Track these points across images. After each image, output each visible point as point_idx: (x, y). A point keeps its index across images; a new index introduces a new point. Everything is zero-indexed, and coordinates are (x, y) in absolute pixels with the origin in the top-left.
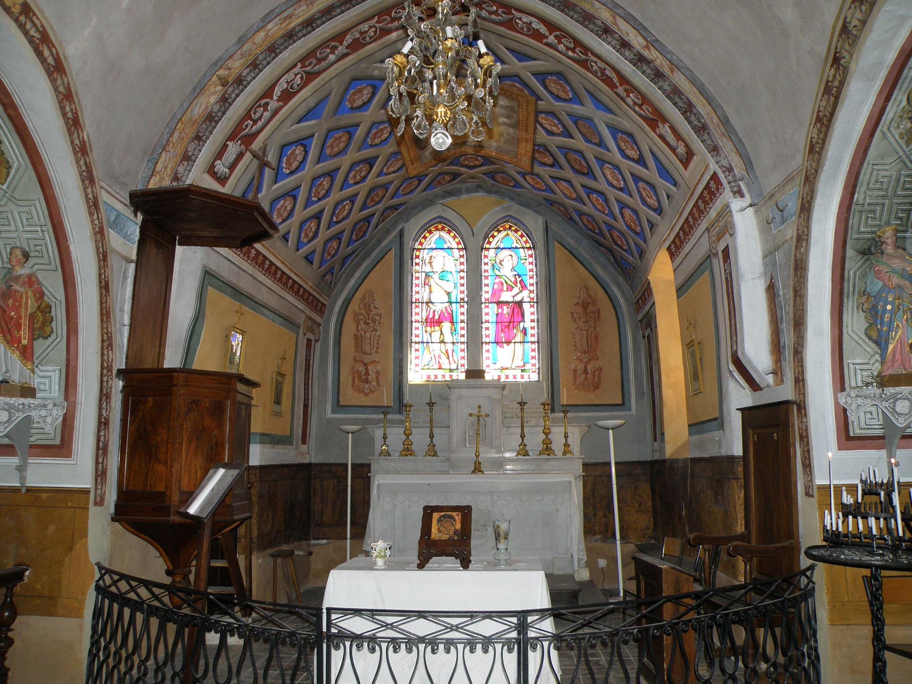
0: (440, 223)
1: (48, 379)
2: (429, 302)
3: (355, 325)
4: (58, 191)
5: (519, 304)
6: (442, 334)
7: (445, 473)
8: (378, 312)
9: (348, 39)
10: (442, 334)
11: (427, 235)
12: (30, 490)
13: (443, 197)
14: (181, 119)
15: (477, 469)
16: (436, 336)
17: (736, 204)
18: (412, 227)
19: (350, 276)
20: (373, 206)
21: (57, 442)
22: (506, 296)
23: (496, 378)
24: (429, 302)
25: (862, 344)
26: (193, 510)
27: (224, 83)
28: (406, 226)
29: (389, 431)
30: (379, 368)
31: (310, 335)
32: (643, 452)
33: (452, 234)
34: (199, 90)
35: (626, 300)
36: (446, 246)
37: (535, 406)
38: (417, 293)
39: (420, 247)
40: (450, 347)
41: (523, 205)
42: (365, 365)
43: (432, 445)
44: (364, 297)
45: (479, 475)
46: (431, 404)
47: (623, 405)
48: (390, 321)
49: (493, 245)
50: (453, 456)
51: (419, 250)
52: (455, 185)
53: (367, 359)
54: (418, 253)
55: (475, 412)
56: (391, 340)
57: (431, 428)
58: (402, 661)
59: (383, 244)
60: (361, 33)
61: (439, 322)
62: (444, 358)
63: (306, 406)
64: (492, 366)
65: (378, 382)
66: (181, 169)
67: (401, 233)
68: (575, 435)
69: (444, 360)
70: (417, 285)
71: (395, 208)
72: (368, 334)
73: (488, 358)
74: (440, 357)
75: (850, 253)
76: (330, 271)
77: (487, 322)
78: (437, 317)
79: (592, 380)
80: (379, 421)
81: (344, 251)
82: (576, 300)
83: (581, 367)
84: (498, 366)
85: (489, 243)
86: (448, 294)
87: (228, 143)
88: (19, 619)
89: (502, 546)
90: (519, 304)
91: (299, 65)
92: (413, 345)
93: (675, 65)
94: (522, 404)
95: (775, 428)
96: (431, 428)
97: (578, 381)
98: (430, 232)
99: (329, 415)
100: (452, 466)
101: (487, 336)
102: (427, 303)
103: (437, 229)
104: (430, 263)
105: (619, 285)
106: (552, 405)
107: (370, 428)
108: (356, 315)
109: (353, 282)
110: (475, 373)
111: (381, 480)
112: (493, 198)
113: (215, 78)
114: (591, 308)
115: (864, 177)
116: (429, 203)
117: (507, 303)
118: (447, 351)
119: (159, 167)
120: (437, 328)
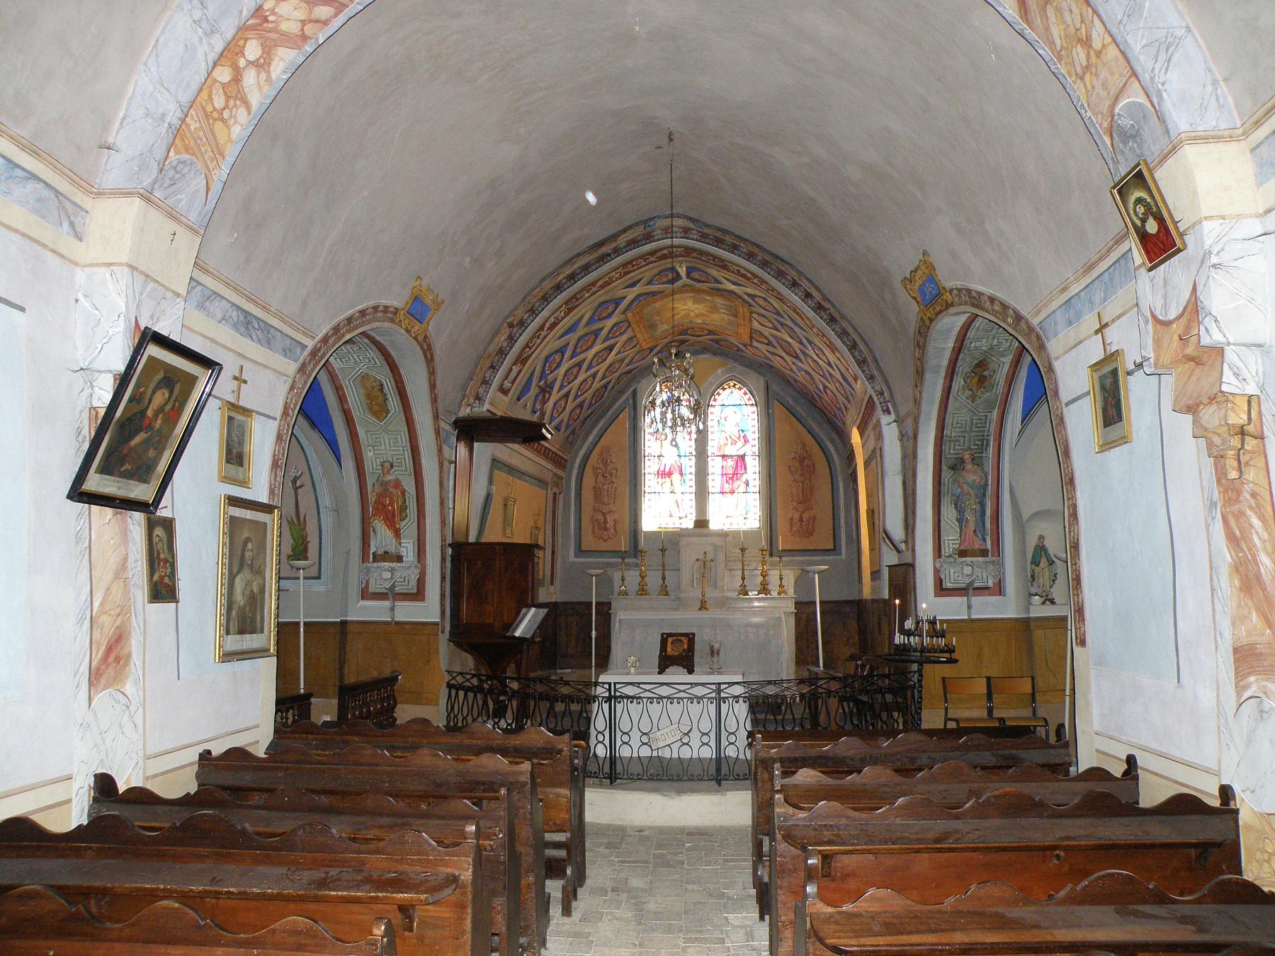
1: (408, 550)
4: (418, 426)
5: (742, 457)
7: (677, 609)
12: (397, 623)
15: (703, 606)
17: (885, 419)
19: (589, 433)
21: (415, 591)
22: (731, 450)
25: (988, 513)
26: (517, 634)
27: (511, 325)
29: (626, 573)
31: (555, 490)
32: (842, 593)
34: (496, 333)
35: (839, 455)
37: (753, 553)
41: (746, 366)
42: (604, 514)
45: (704, 612)
46: (663, 550)
47: (835, 550)
49: (719, 402)
50: (682, 595)
55: (701, 557)
56: (627, 491)
57: (664, 570)
58: (655, 708)
61: (670, 474)
63: (553, 552)
66: (481, 390)
68: (790, 578)
75: (944, 468)
76: (573, 433)
79: (806, 528)
80: (617, 564)
81: (585, 413)
82: (793, 455)
83: (797, 516)
88: (399, 706)
89: (715, 659)
90: (742, 457)
93: (843, 316)
94: (743, 550)
95: (903, 579)
96: (664, 570)
97: (795, 529)
99: (572, 558)
100: (681, 603)
105: (833, 442)
106: (771, 550)
107: (610, 571)
108: (595, 469)
109: (591, 438)
110: (701, 523)
111: (622, 615)
112: (717, 359)
114: (806, 462)
115: (948, 421)
117: (732, 456)
120: (668, 480)
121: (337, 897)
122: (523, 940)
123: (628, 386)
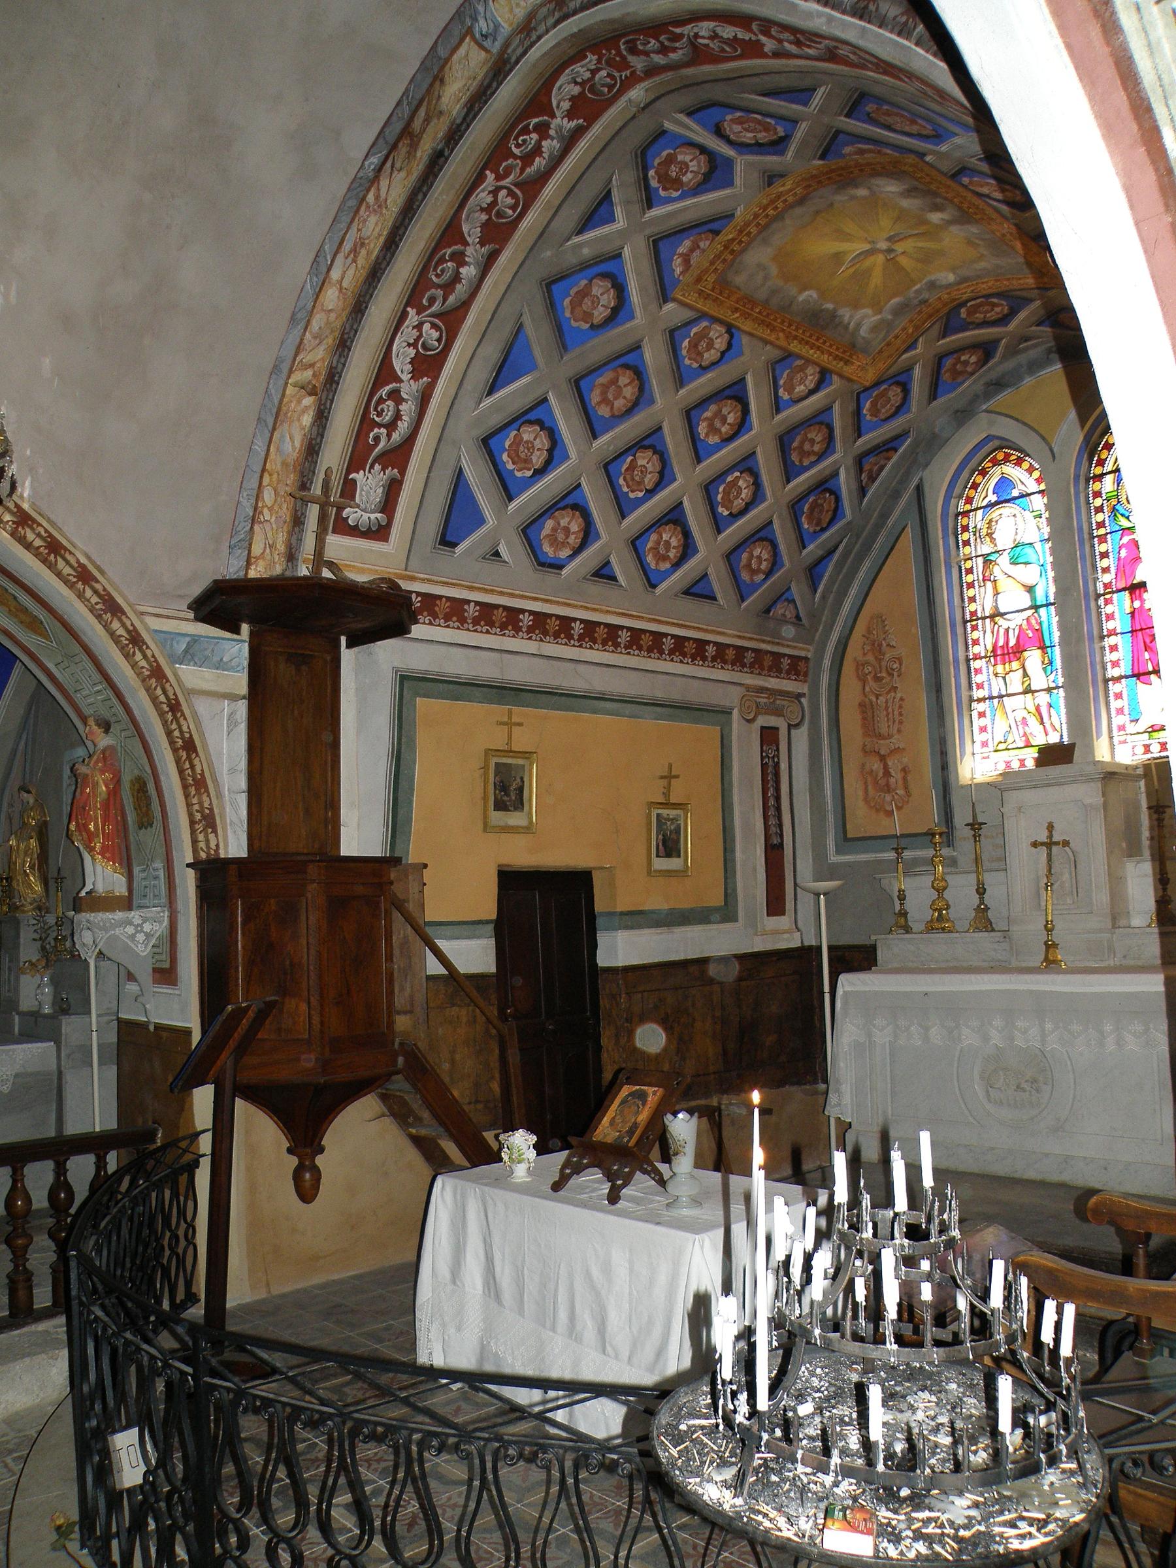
0: (1000, 448)
2: (996, 614)
3: (860, 684)
6: (1025, 675)
8: (895, 653)
9: (471, 229)
10: (1025, 675)
11: (979, 479)
13: (987, 396)
14: (264, 470)
16: (1015, 682)
18: (938, 477)
20: (813, 464)
23: (1001, 768)
24: (996, 614)
28: (927, 472)
30: (905, 760)
33: (1025, 465)
36: (1015, 493)
38: (973, 599)
39: (968, 507)
40: (1043, 699)
42: (883, 758)
43: (982, 911)
44: (869, 631)
48: (918, 668)
51: (966, 514)
52: (997, 366)
53: (884, 747)
54: (965, 521)
55: (1043, 837)
56: (922, 702)
59: (890, 522)
60: (488, 209)
62: (1033, 722)
64: (1131, 728)
65: (906, 788)
67: (919, 489)
69: (1034, 725)
70: (971, 585)
71: (887, 447)
72: (882, 699)
73: (1120, 711)
74: (1024, 722)
77: (1113, 633)
78: (1012, 642)
84: (1143, 725)
85: (1101, 463)
86: (1030, 589)
87: (358, 476)
91: (411, 312)
92: (974, 705)
98: (984, 473)
101: (1116, 664)
102: (992, 617)
103: (995, 463)
104: (990, 535)
108: (859, 666)
113: (290, 390)
116: (963, 416)
118: (1038, 708)
119: (257, 550)
120: (1015, 665)
121: (1149, 1483)
122: (974, 1448)
123: (907, 476)
